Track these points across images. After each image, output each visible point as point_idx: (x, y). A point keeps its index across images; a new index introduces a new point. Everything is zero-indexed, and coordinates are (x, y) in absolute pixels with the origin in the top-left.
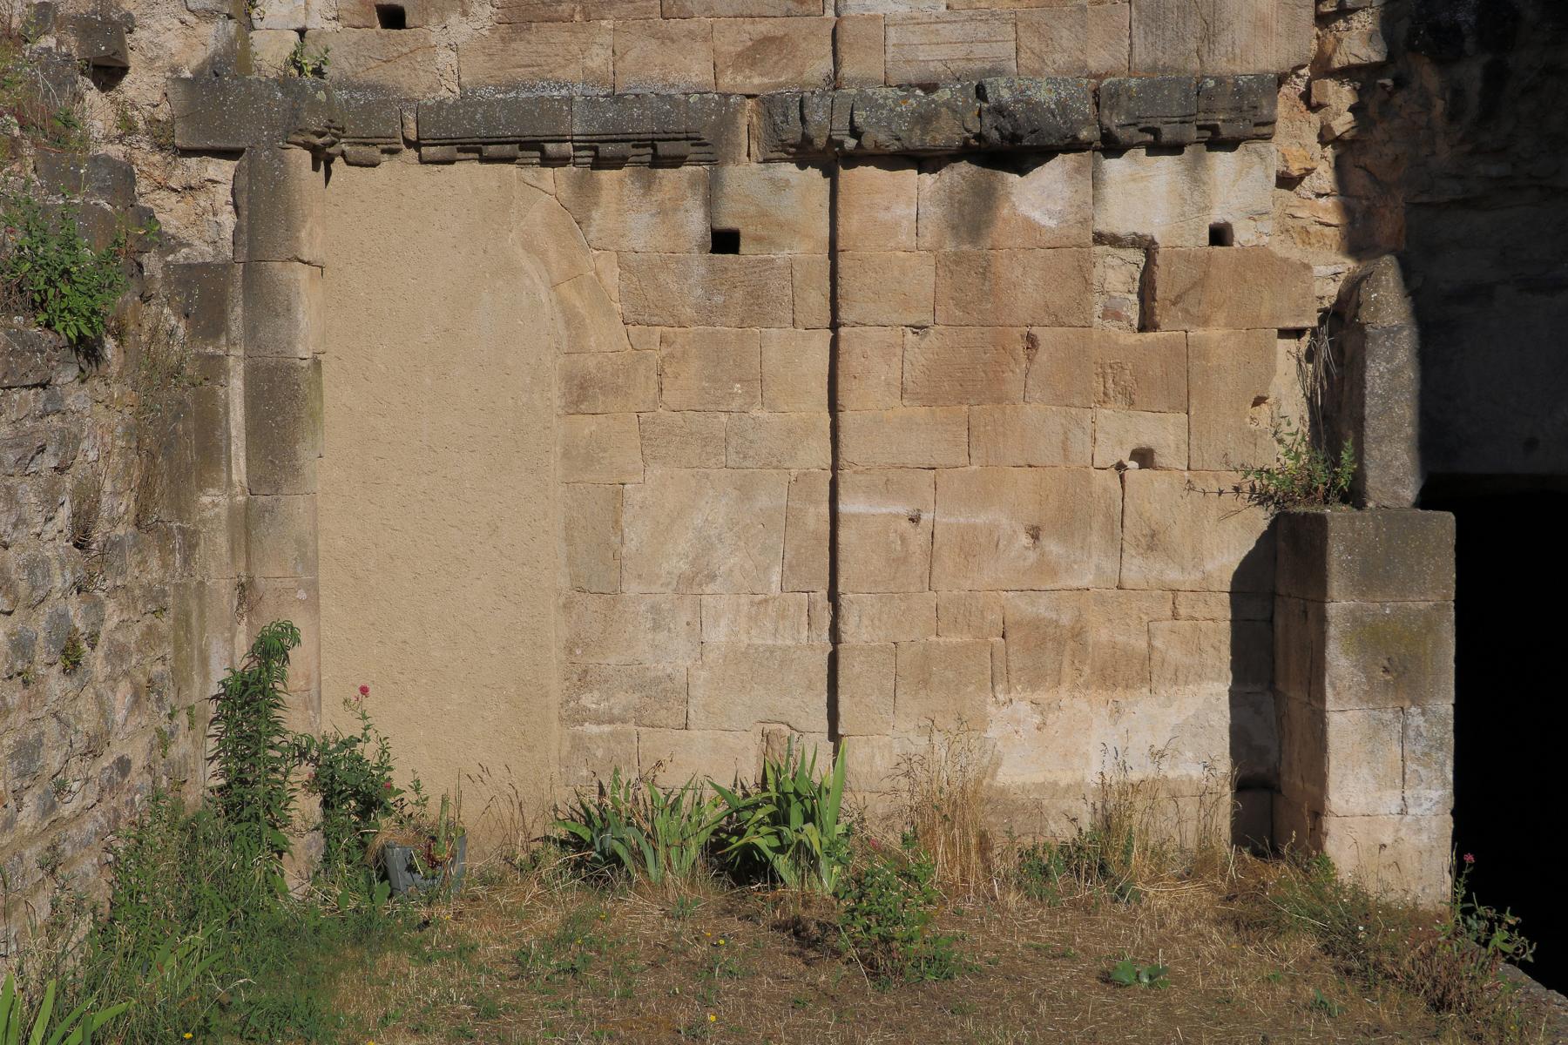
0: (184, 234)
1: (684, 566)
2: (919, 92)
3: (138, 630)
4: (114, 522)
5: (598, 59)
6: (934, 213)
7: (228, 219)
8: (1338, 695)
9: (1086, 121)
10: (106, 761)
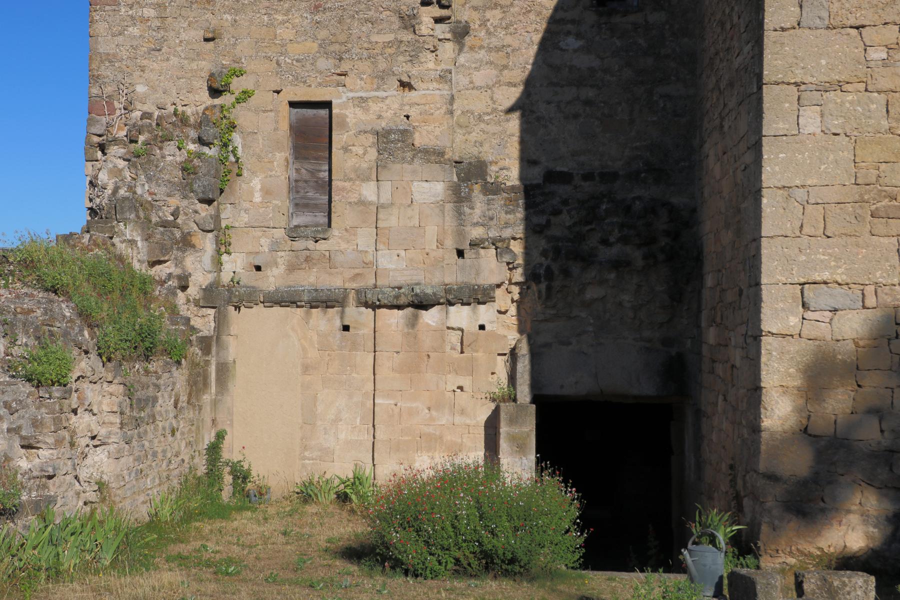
0: (201, 328)
1: (333, 417)
2: (397, 290)
3: (187, 429)
4: (183, 402)
5: (312, 279)
6: (402, 321)
7: (213, 324)
8: (503, 454)
9: (442, 297)
10: (180, 458)
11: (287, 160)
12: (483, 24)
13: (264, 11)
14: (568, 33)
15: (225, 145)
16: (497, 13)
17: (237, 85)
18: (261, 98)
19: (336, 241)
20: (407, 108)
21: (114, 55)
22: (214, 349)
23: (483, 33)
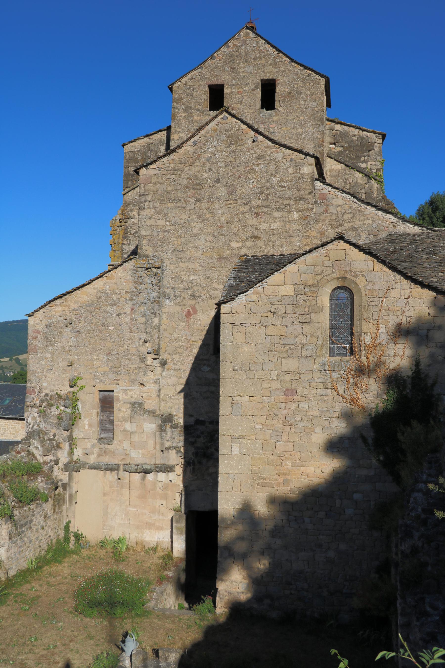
5: (107, 460)
7: (68, 478)
11: (98, 413)
12: (172, 360)
13: (89, 355)
14: (205, 365)
15: (74, 408)
16: (178, 356)
17: (79, 383)
18: (88, 388)
19: (115, 446)
20: (142, 394)
21: (36, 371)
22: (68, 488)
23: (172, 364)
